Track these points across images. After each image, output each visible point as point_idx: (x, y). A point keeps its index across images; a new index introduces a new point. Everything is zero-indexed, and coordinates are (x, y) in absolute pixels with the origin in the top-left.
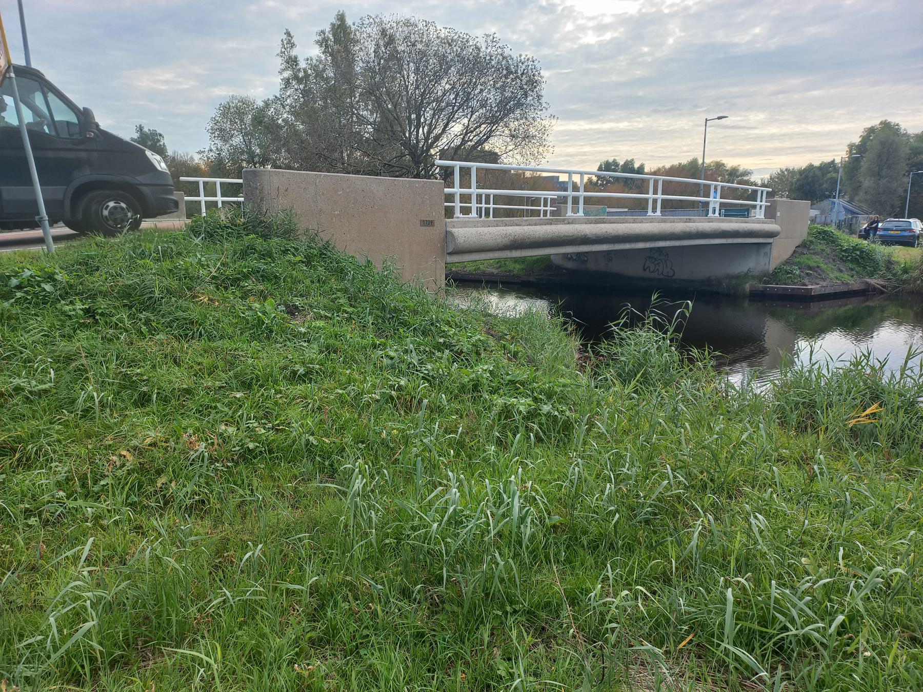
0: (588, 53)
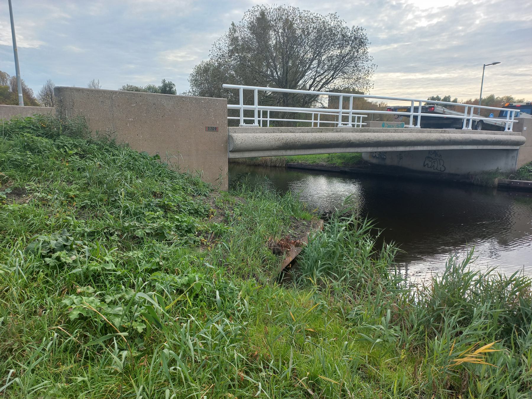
0: (422, 33)
